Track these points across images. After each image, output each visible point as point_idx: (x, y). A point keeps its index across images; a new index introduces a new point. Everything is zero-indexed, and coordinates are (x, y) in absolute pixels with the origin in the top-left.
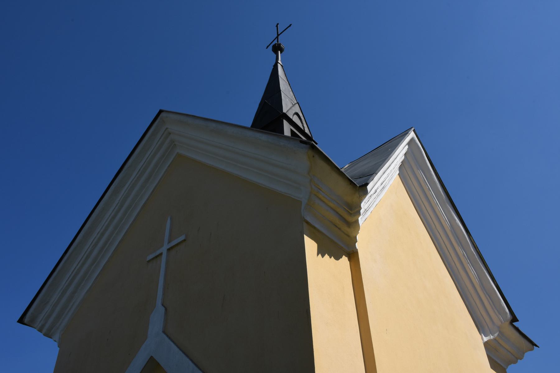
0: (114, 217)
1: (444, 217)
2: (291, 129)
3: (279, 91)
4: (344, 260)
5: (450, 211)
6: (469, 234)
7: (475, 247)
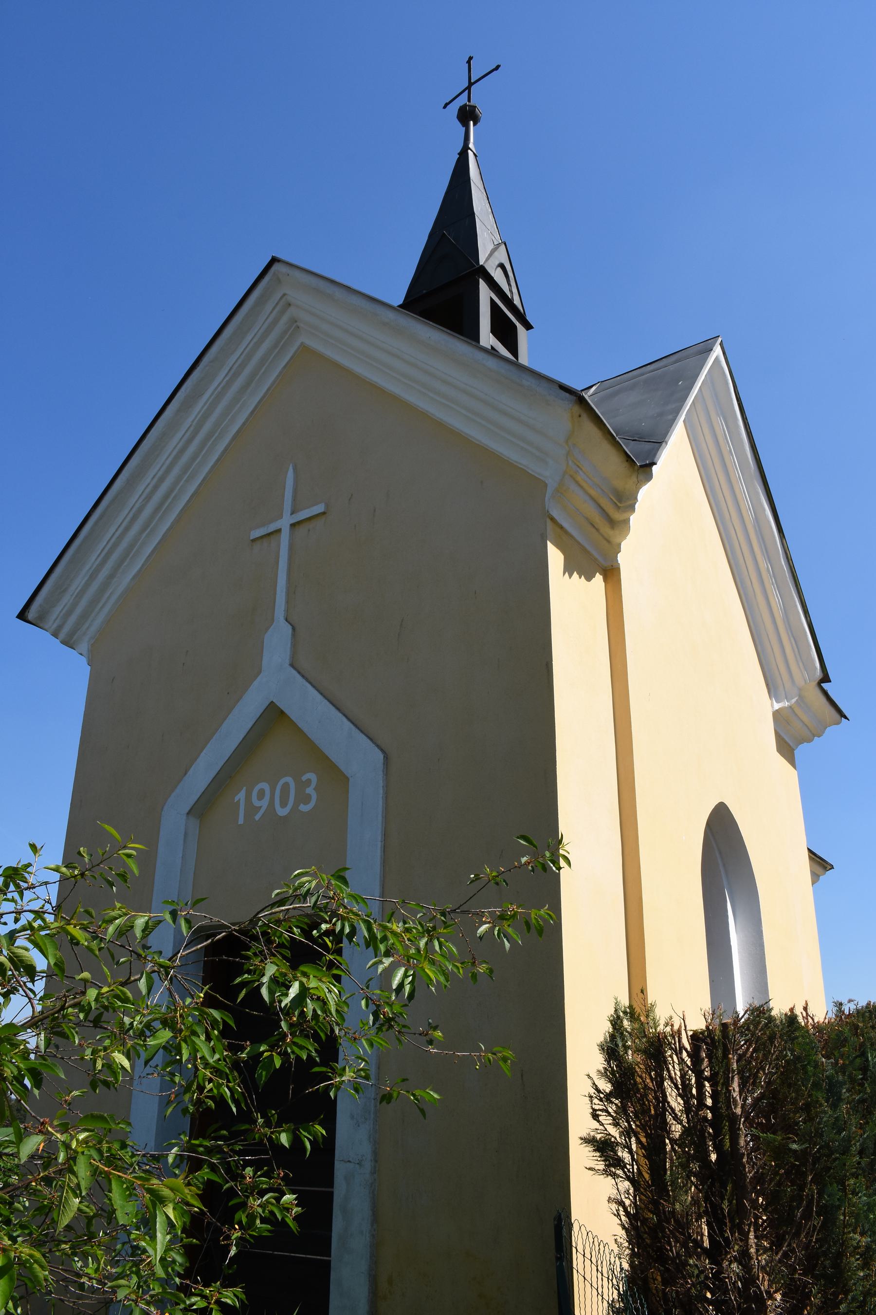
0: (182, 451)
1: (746, 504)
2: (491, 298)
3: (472, 215)
4: (599, 578)
5: (758, 493)
6: (781, 535)
7: (787, 558)
